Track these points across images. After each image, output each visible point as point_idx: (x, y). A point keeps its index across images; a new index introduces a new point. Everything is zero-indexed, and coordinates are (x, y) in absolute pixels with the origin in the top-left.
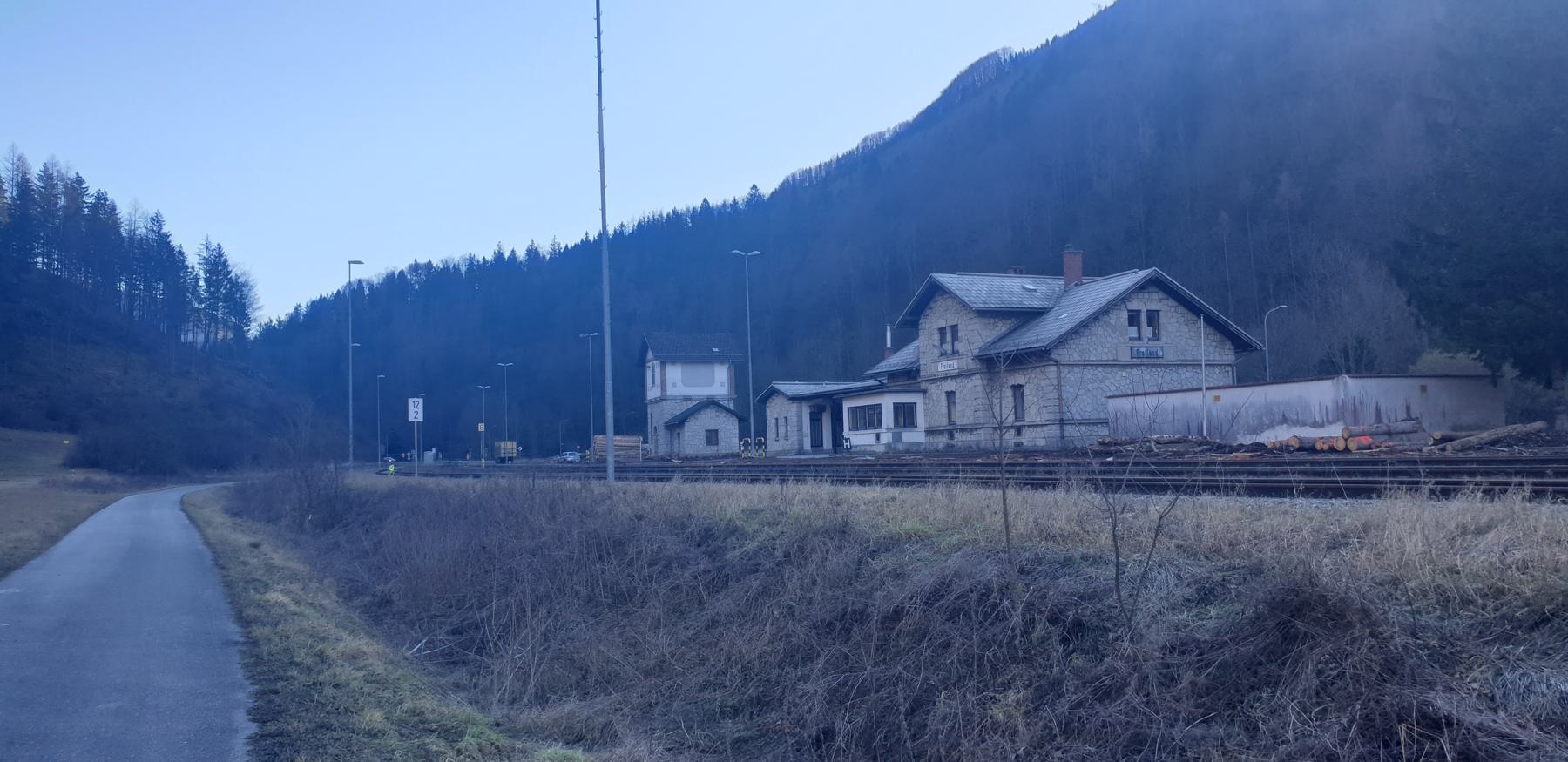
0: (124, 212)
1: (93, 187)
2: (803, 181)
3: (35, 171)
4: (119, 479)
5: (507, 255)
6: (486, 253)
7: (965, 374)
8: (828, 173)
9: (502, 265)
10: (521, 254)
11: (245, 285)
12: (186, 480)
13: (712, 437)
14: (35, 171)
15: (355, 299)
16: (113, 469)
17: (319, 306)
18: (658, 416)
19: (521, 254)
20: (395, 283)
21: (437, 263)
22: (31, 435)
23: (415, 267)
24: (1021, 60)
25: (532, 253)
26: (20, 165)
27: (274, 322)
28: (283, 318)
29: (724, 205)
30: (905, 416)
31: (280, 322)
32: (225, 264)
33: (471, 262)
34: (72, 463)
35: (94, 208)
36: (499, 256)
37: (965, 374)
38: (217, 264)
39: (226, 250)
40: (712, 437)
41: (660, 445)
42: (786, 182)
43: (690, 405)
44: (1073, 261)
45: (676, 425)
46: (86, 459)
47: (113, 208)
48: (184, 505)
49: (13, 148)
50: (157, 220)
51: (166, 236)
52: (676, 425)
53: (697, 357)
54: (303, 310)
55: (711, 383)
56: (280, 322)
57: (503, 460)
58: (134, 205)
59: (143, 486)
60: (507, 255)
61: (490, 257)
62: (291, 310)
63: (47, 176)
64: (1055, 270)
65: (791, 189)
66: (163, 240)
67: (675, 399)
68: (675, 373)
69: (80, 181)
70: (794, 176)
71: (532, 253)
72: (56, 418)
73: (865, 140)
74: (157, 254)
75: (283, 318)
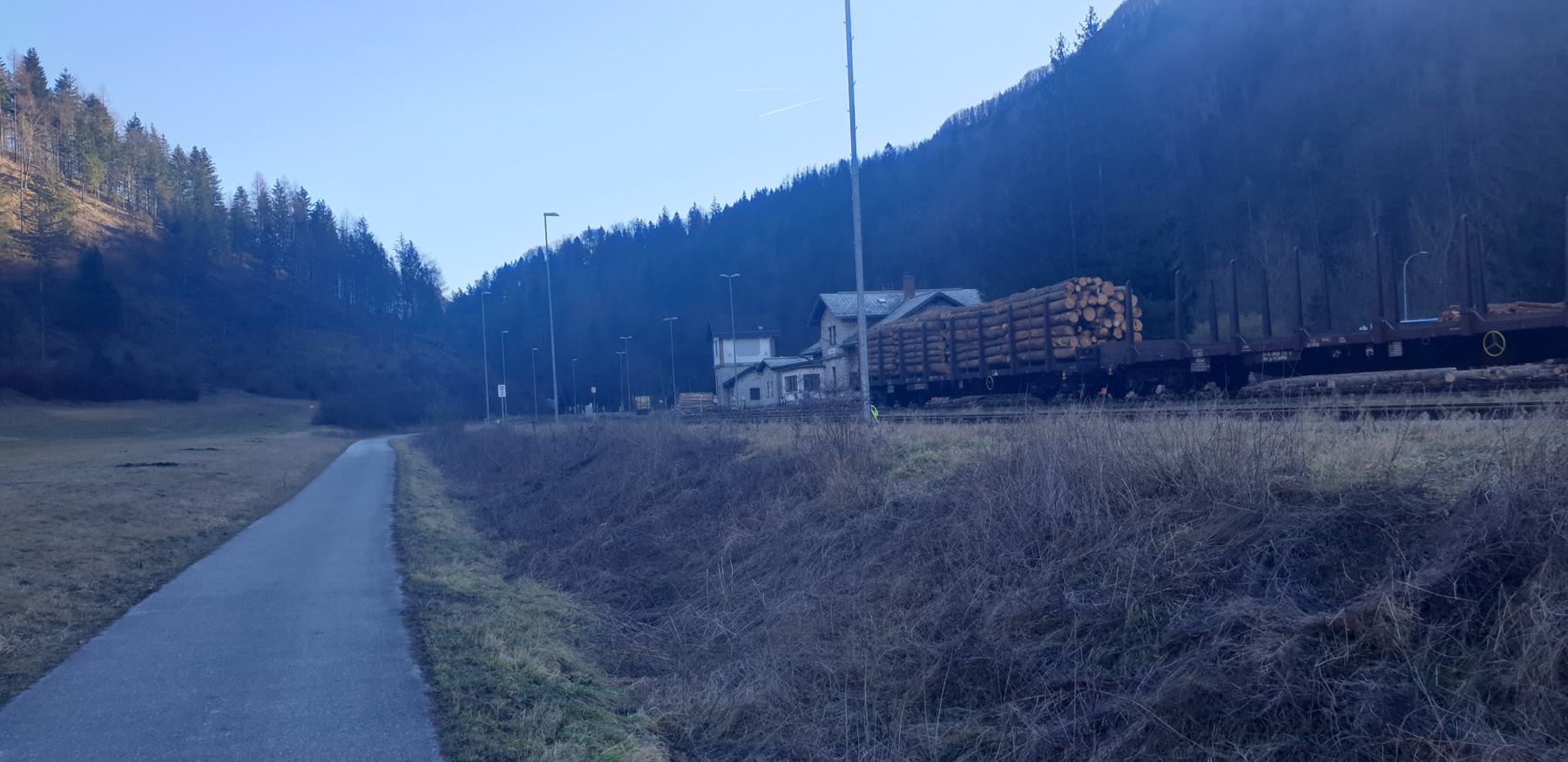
0: (337, 216)
1: (314, 198)
2: (963, 121)
3: (271, 186)
4: (351, 432)
5: (671, 218)
6: (652, 218)
7: (838, 357)
8: (990, 111)
9: (668, 227)
10: (684, 217)
11: (434, 271)
12: (394, 432)
13: (755, 393)
14: (271, 186)
15: (535, 266)
16: (345, 425)
17: (505, 273)
18: (722, 376)
19: (684, 217)
20: (571, 248)
21: (608, 229)
22: (288, 402)
23: (589, 233)
24: (781, 194)
25: (695, 214)
26: (259, 182)
27: (465, 290)
28: (473, 285)
29: (876, 155)
30: (812, 382)
31: (470, 290)
32: (416, 257)
33: (639, 226)
34: (318, 422)
35: (315, 214)
36: (664, 220)
37: (838, 357)
38: (409, 256)
39: (415, 245)
40: (755, 393)
41: (719, 400)
42: (948, 122)
43: (741, 370)
44: (908, 281)
45: (730, 385)
46: (328, 418)
47: (330, 213)
48: (389, 443)
49: (258, 176)
50: (362, 224)
51: (370, 237)
52: (730, 385)
53: (747, 333)
54: (491, 277)
55: (757, 353)
56: (470, 290)
57: (640, 412)
58: (346, 211)
59: (365, 437)
60: (671, 218)
61: (655, 222)
62: (480, 277)
63: (279, 190)
64: (898, 287)
65: (952, 130)
66: (367, 239)
67: (730, 366)
68: (729, 346)
69: (304, 193)
70: (955, 117)
71: (695, 214)
72: (301, 388)
73: (1027, 76)
74: (365, 249)
75: (473, 285)
